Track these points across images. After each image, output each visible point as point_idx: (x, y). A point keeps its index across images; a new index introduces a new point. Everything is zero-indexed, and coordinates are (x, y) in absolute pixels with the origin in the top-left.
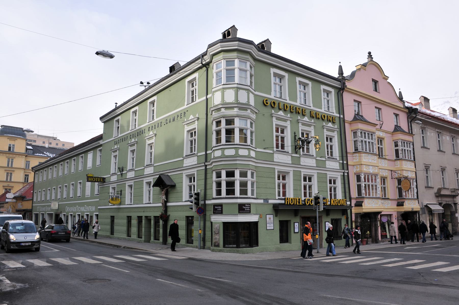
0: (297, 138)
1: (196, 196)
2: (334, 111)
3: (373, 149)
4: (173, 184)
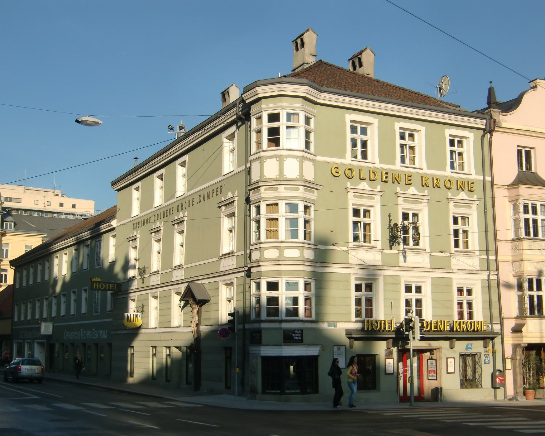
2: (473, 171)
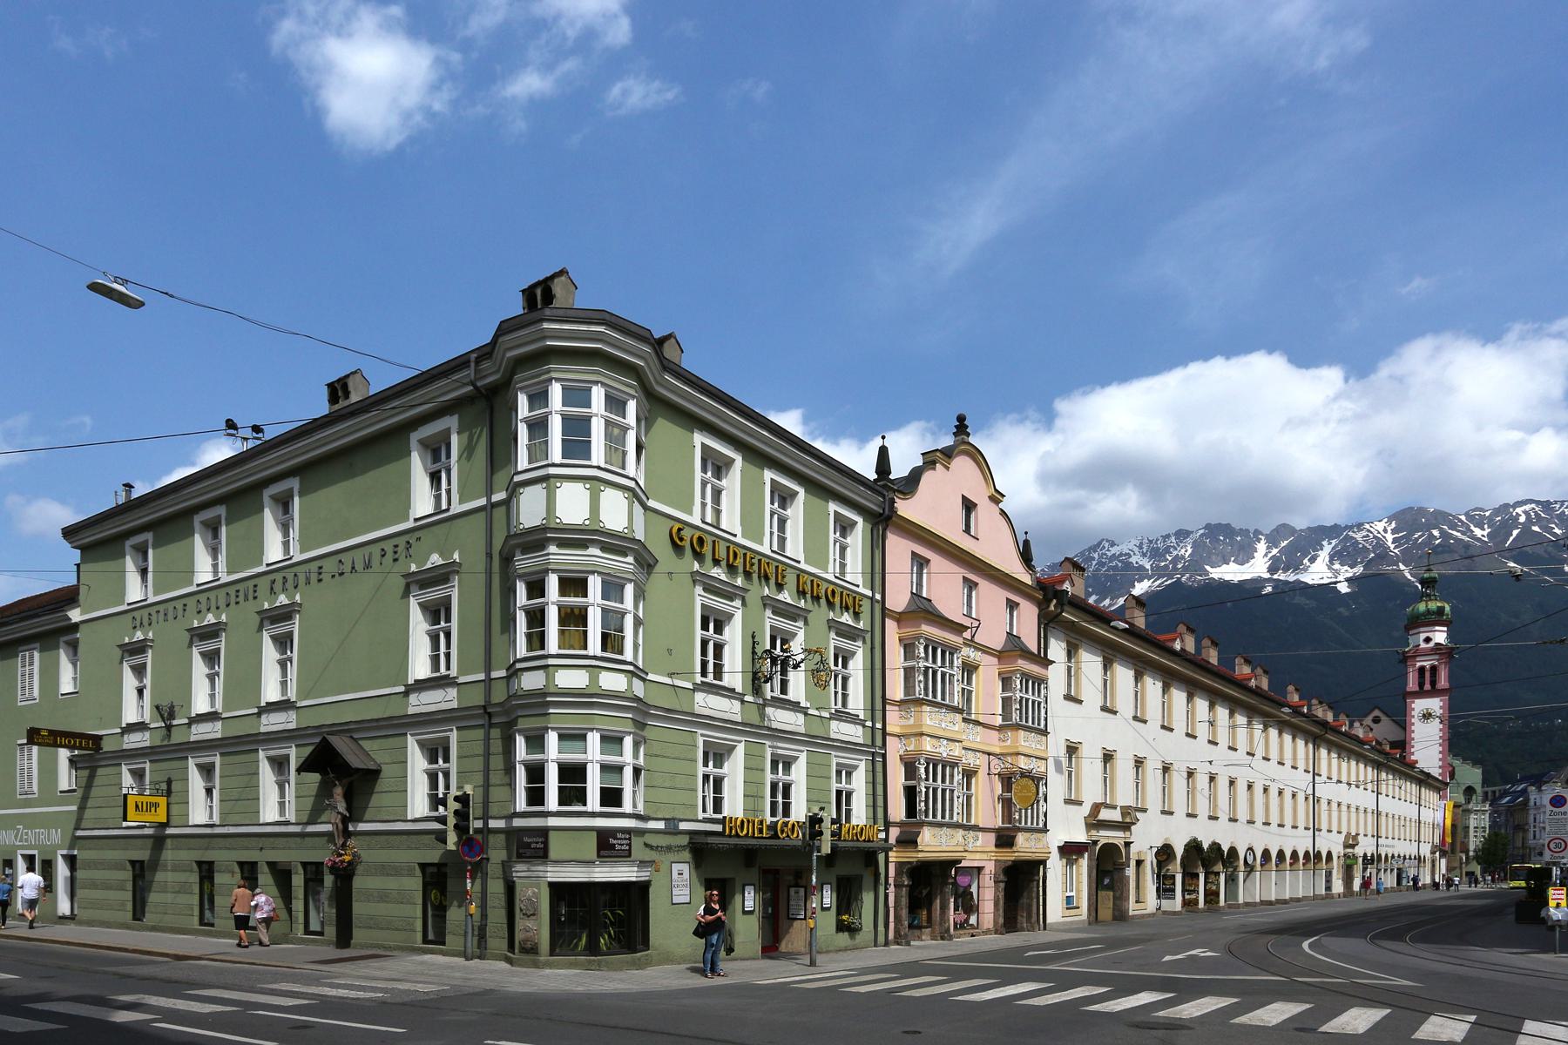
0: (759, 650)
1: (457, 806)
2: (860, 582)
3: (952, 694)
4: (372, 766)
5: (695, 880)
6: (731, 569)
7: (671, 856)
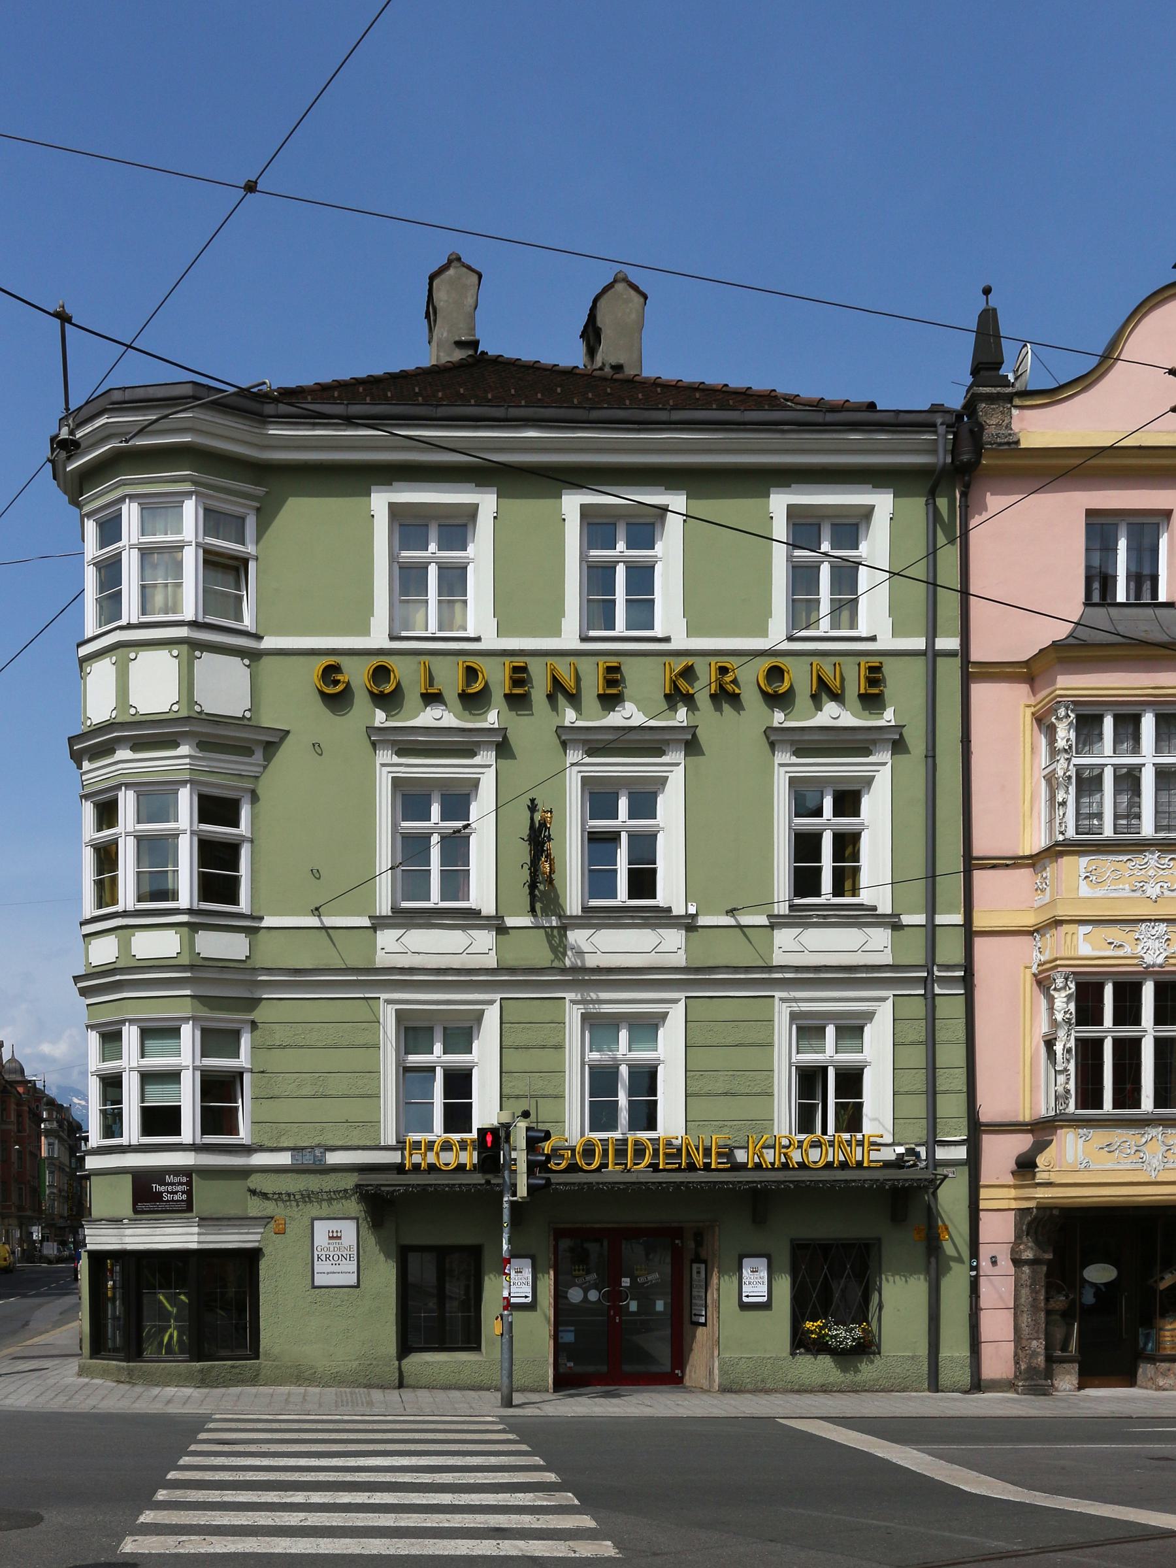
5: (371, 1241)
6: (474, 701)
7: (314, 1210)
